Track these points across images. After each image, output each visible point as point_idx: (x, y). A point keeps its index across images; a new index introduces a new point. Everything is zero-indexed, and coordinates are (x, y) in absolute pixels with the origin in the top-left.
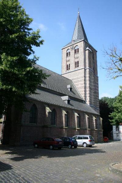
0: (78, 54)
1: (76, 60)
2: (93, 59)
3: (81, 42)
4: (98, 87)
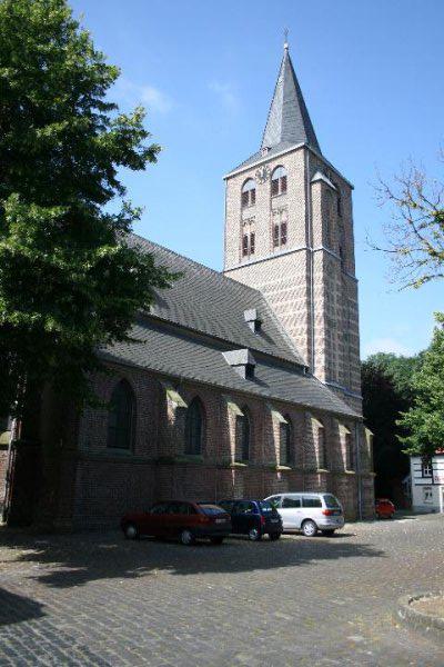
1: (278, 220)
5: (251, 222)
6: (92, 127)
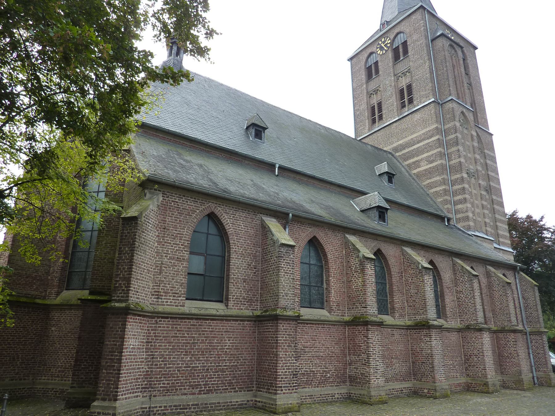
0: (406, 60)
1: (403, 82)
2: (467, 74)
3: (413, 17)
5: (376, 91)
6: (196, 26)
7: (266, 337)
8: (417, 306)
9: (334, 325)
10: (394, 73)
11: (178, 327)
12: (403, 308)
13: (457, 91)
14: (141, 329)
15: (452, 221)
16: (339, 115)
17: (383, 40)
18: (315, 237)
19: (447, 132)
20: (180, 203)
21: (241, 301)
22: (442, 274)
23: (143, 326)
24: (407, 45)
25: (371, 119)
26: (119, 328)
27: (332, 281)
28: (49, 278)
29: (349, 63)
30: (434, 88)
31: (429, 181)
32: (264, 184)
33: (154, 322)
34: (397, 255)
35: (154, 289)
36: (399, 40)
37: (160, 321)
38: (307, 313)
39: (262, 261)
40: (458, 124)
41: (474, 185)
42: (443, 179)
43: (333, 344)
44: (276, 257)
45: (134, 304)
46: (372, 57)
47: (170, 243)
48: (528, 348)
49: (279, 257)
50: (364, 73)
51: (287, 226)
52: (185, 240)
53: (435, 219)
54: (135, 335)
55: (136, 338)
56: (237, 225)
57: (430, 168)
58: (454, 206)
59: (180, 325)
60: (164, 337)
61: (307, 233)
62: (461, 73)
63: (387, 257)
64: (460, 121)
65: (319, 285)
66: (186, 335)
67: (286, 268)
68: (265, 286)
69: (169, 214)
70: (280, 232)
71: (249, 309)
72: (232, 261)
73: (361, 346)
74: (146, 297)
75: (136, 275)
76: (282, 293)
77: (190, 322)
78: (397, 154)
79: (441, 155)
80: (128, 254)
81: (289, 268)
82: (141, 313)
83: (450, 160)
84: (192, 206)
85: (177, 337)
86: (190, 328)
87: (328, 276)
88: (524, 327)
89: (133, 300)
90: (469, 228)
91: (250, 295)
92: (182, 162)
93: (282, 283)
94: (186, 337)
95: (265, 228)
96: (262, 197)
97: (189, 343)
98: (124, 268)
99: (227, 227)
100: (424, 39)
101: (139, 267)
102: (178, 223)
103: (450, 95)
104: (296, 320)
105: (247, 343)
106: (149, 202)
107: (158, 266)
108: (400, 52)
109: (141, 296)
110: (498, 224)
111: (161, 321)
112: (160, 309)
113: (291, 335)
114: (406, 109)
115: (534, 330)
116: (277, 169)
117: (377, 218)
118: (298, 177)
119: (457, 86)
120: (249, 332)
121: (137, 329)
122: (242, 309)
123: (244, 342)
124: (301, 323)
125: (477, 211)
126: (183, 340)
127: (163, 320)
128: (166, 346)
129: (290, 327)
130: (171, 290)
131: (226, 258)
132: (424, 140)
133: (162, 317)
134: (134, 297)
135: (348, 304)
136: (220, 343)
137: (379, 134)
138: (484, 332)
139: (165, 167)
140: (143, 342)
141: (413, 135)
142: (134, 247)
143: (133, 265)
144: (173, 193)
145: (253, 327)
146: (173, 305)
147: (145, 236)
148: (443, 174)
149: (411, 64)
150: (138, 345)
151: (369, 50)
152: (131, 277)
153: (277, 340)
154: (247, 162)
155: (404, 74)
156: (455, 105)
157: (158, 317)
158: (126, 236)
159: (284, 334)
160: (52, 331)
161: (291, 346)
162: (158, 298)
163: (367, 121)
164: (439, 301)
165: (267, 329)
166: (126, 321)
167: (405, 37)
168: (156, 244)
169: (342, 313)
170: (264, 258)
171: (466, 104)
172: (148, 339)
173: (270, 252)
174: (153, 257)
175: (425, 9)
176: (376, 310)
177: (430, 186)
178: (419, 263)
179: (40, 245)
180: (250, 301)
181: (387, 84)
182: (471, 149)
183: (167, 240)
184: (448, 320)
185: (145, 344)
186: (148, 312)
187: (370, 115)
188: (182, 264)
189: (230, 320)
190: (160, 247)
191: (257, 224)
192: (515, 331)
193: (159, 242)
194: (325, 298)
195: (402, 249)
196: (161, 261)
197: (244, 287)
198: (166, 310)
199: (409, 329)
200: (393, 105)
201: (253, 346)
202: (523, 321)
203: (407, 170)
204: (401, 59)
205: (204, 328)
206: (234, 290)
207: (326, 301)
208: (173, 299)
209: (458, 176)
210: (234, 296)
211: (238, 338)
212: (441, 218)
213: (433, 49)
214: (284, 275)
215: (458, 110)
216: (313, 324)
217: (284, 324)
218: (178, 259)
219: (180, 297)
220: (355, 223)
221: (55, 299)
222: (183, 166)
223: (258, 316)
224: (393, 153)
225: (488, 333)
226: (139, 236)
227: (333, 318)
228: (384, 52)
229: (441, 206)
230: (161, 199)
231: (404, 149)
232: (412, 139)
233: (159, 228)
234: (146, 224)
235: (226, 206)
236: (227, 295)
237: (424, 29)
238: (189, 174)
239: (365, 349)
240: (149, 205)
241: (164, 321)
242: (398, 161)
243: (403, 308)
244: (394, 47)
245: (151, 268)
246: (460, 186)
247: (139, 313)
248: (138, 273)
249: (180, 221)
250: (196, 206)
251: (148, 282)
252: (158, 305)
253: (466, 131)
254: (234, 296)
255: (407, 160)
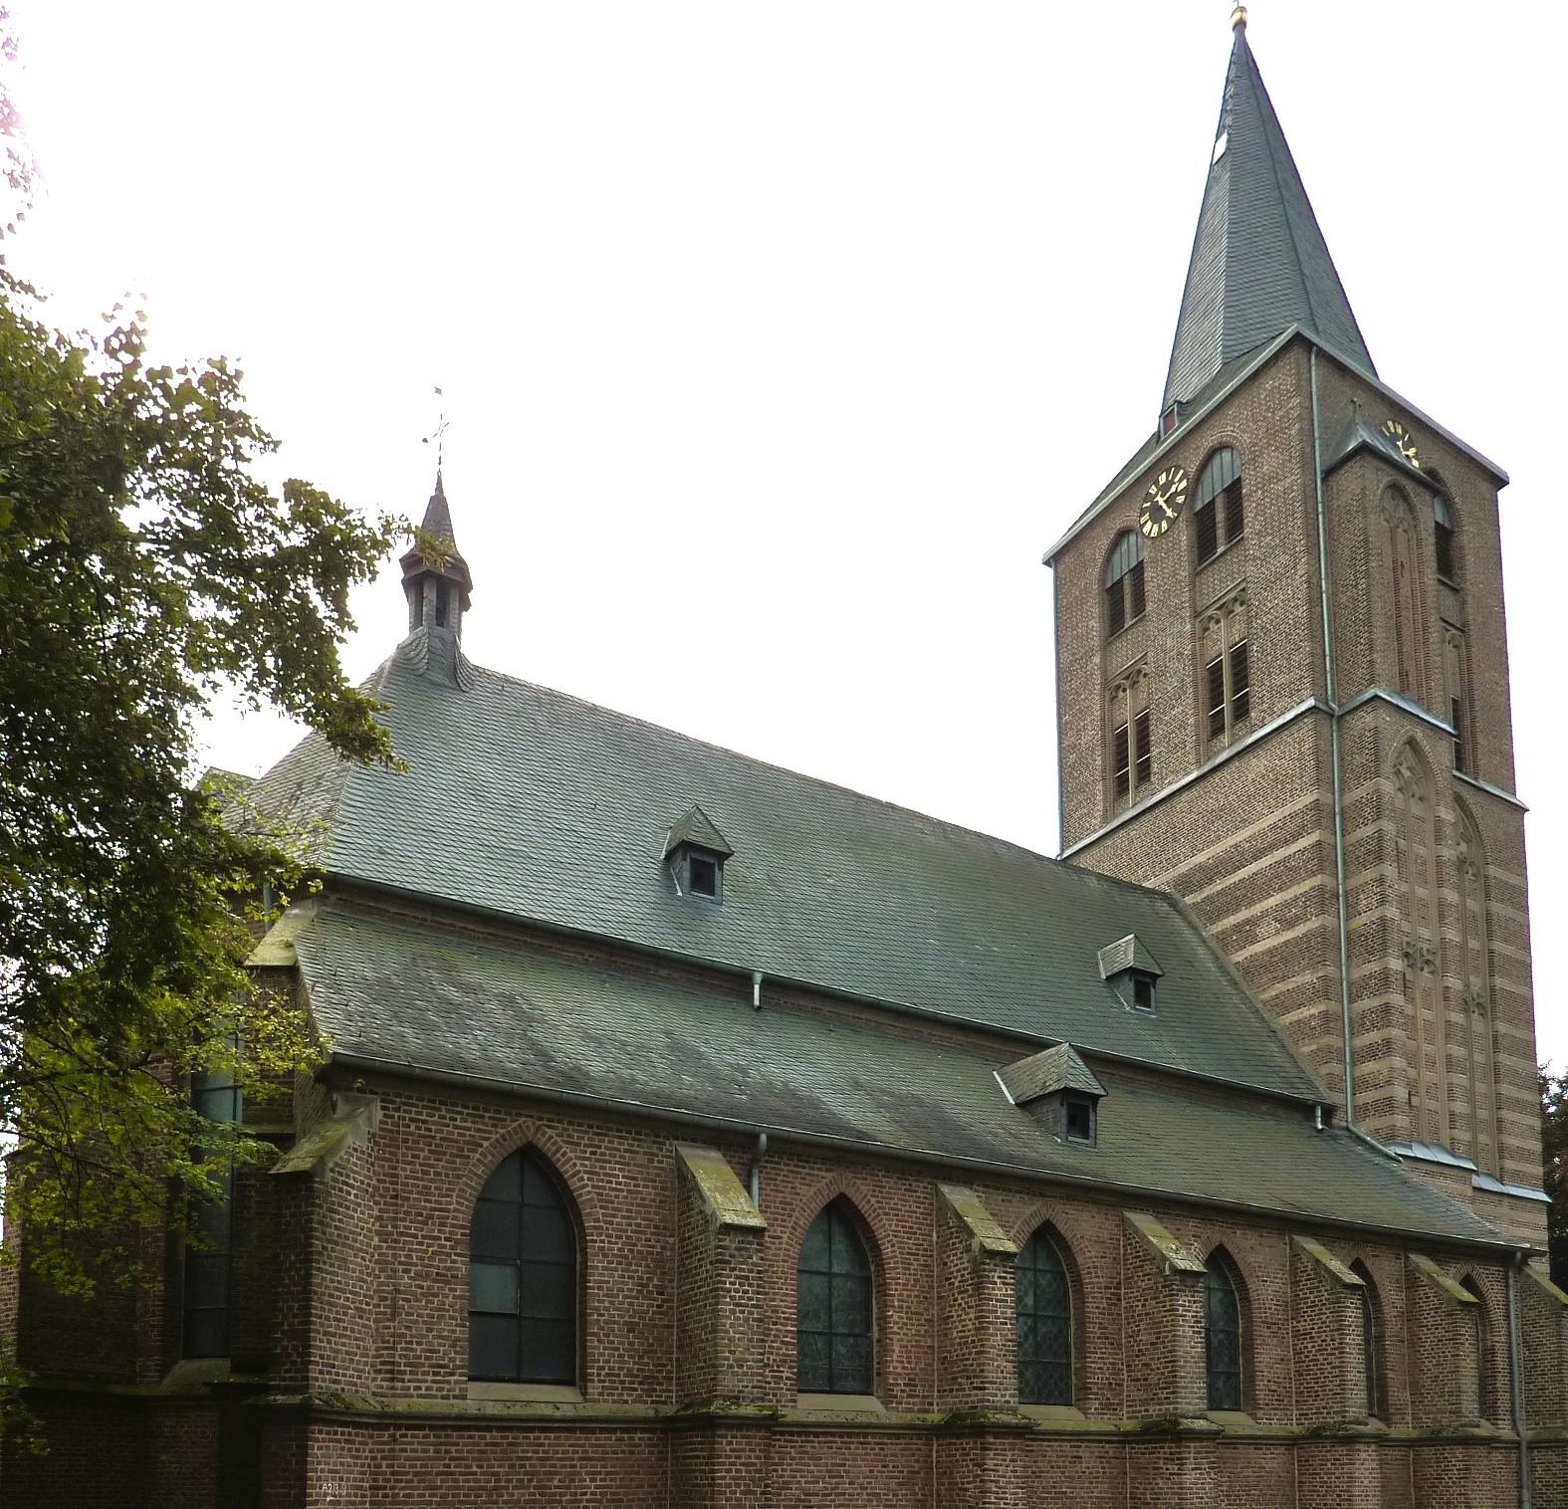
1: (1222, 640)
3: (1268, 383)
4: (1526, 927)
5: (1134, 676)
7: (689, 1471)
8: (1153, 1379)
9: (897, 1436)
10: (1193, 607)
11: (454, 1449)
12: (1115, 1387)
13: (1401, 662)
14: (353, 1457)
15: (1340, 1114)
16: (996, 771)
17: (1163, 479)
18: (842, 1196)
19: (1350, 818)
20: (434, 1123)
21: (623, 1382)
22: (1252, 1284)
23: (358, 1450)
24: (1240, 496)
25: (1111, 777)
26: (293, 1455)
27: (895, 1318)
28: (137, 1328)
29: (1049, 572)
30: (1318, 661)
31: (1280, 987)
32: (707, 1042)
33: (386, 1439)
34: (1106, 1235)
35: (382, 1356)
36: (1217, 477)
37: (402, 1436)
38: (813, 1407)
39: (680, 1273)
40: (1387, 787)
41: (1427, 993)
42: (1324, 978)
43: (894, 1486)
44: (711, 1263)
45: (324, 1397)
46: (1124, 547)
47: (415, 1236)
48: (1520, 1488)
49: (717, 1261)
50: (1096, 611)
51: (756, 1171)
52: (453, 1225)
53: (1281, 1112)
54: (336, 1472)
55: (341, 1479)
56: (604, 1180)
57: (1286, 943)
58: (1354, 1064)
59: (458, 1445)
60: (416, 1474)
61: (814, 1189)
62: (1423, 592)
63: (1075, 1245)
64: (1398, 773)
65: (857, 1331)
66: (475, 1469)
67: (737, 1291)
68: (686, 1341)
69: (405, 1155)
70: (724, 1191)
71: (646, 1402)
72: (593, 1279)
73: (966, 1490)
74: (359, 1377)
75: (322, 1325)
76: (727, 1359)
77: (484, 1438)
78: (1189, 900)
79: (1323, 899)
80: (298, 1271)
81: (746, 1292)
82: (341, 1416)
83: (1352, 911)
84: (469, 1129)
85: (452, 1474)
86: (485, 1452)
87: (884, 1306)
88: (1515, 1427)
89: (321, 1387)
90: (1391, 1137)
91: (647, 1364)
92: (454, 994)
93: (727, 1332)
94: (475, 1474)
95: (685, 1179)
96: (689, 1085)
97: (484, 1489)
98: (290, 1309)
99: (574, 1183)
100: (1296, 467)
101: (329, 1304)
102: (430, 1181)
103: (1372, 681)
104: (768, 1428)
105: (642, 1486)
106: (343, 1129)
107: (386, 1298)
108: (1215, 526)
109: (344, 1375)
110: (1506, 1114)
111: (406, 1436)
112: (400, 1406)
113: (754, 1464)
114: (1225, 739)
115: (1546, 1435)
116: (757, 987)
117: (1063, 1126)
118: (827, 1008)
119: (1400, 646)
120: (648, 1459)
121: (341, 1456)
122: (626, 1402)
123: (634, 1484)
124: (782, 1433)
125: (1429, 1076)
126: (468, 1481)
127: (410, 1433)
128: (424, 1495)
129: (749, 1444)
130: (427, 1358)
131: (578, 1268)
132: (1272, 847)
133: (408, 1427)
134: (324, 1380)
135: (940, 1380)
136: (567, 1487)
137: (1133, 832)
138: (1362, 1447)
139: (395, 1015)
140: (361, 1488)
141: (1243, 823)
142: (311, 1253)
143: (311, 1299)
144: (411, 1098)
145: (657, 1446)
146: (436, 1397)
147: (340, 1221)
148: (1323, 962)
149: (1251, 570)
150: (348, 1495)
151: (1116, 524)
152: (309, 1331)
153: (713, 1479)
154: (663, 972)
155: (1226, 609)
156: (1385, 717)
157: (398, 1427)
158: (288, 1224)
159: (731, 1464)
160: (163, 1462)
161: (753, 1493)
162: (392, 1380)
163: (1100, 787)
164: (1237, 1364)
165: (692, 1450)
166: (307, 1439)
167: (1237, 463)
168: (376, 1239)
169: (923, 1404)
170: (684, 1265)
171: (1428, 711)
172: (374, 1480)
173: (696, 1248)
174: (369, 1275)
175: (1309, 345)
176: (1011, 1396)
177: (1283, 1004)
178: (1164, 1258)
179: (84, 1243)
180: (649, 1381)
181: (1168, 643)
182: (1431, 868)
183: (405, 1227)
184: (1260, 1414)
185: (368, 1493)
186: (369, 1416)
187: (1111, 762)
188: (450, 1290)
189: (592, 1431)
190: (388, 1248)
191: (664, 1169)
192: (1468, 1441)
193: (384, 1236)
194: (876, 1366)
195: (1124, 1220)
196: (394, 1285)
197: (631, 1344)
198: (415, 1409)
199: (1129, 1442)
200: (1182, 727)
201: (660, 1492)
202: (1513, 1412)
203: (1213, 954)
204: (1220, 550)
205: (523, 1451)
206: (601, 1355)
207: (878, 1374)
208: (433, 1382)
209: (1373, 967)
210: (603, 1368)
211: (617, 1473)
212: (1302, 1109)
213: (1328, 510)
214: (733, 1312)
215: (1394, 733)
216: (833, 1434)
217: (733, 1437)
218: (440, 1277)
219: (452, 1374)
220: (979, 1148)
221: (158, 1383)
222: (449, 1008)
223: (669, 1419)
224: (1177, 896)
225: (1373, 1447)
226: (321, 1223)
227: (894, 1418)
228: (1164, 526)
229: (1309, 1069)
230: (379, 1114)
231: (1211, 881)
232: (1236, 846)
233: (381, 1196)
234: (341, 1190)
235: (570, 1123)
236: (584, 1367)
237: (1301, 429)
238: (465, 1030)
239: (975, 1497)
240: (343, 1137)
241: (413, 1436)
242: (1190, 924)
243: (1115, 1387)
244: (1199, 506)
245: (368, 1304)
246: (1376, 1002)
247: (341, 1418)
248: (327, 1318)
249: (437, 1174)
250: (479, 1130)
251: (363, 1340)
252: (393, 1396)
253: (1417, 809)
254: (603, 1368)
255: (1218, 918)
